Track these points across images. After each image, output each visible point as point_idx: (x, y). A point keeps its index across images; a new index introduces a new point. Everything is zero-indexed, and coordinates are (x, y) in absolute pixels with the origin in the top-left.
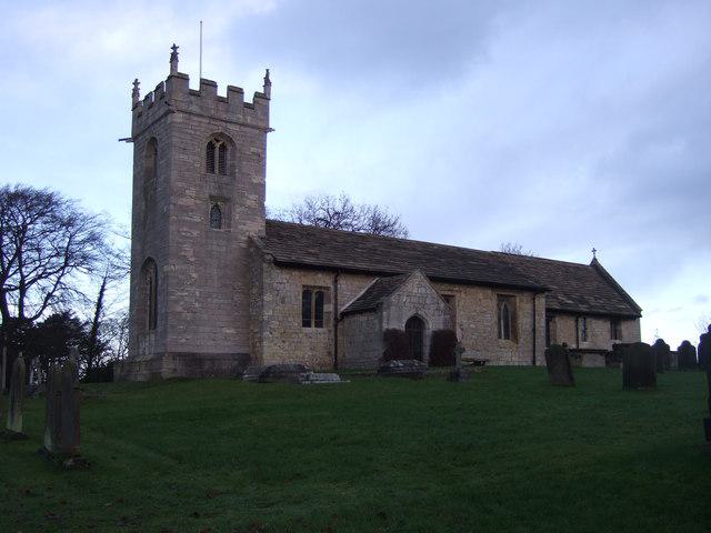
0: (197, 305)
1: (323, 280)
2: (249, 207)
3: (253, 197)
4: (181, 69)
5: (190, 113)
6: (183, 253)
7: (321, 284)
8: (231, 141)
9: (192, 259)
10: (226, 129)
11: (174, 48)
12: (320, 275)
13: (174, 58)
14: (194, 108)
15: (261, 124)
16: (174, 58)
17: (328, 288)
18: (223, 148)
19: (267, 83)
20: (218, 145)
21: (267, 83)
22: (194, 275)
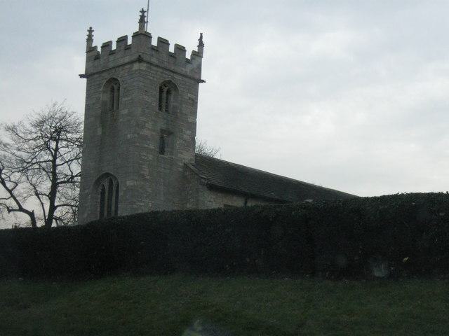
2: (185, 141)
5: (151, 64)
6: (142, 173)
8: (175, 88)
9: (148, 177)
10: (173, 78)
11: (201, 34)
12: (235, 198)
13: (142, 21)
14: (154, 60)
15: (197, 77)
16: (142, 21)
18: (168, 92)
19: (201, 45)
20: (165, 89)
21: (201, 45)
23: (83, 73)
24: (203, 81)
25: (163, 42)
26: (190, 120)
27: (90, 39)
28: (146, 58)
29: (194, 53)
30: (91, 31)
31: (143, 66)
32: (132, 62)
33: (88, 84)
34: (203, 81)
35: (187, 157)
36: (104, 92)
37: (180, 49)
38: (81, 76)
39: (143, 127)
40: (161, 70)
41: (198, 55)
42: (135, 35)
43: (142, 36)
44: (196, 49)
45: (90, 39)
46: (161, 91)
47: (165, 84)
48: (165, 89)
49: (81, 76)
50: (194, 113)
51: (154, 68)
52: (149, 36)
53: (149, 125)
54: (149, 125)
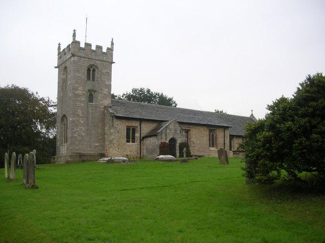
0: (83, 134)
1: (135, 124)
3: (106, 90)
4: (77, 39)
5: (80, 57)
7: (134, 125)
11: (74, 31)
13: (74, 35)
15: (110, 61)
16: (74, 35)
17: (137, 127)
18: (94, 70)
19: (112, 44)
20: (92, 69)
21: (112, 44)
22: (82, 122)
23: (57, 66)
24: (114, 63)
25: (88, 45)
26: (107, 83)
27: (59, 48)
28: (76, 54)
29: (108, 49)
30: (59, 44)
31: (76, 58)
32: (71, 57)
33: (59, 72)
34: (114, 63)
35: (107, 102)
36: (63, 74)
37: (99, 48)
38: (56, 67)
39: (77, 89)
40: (87, 59)
41: (110, 50)
42: (108, 49)
43: (76, 43)
44: (110, 47)
45: (59, 48)
46: (89, 70)
47: (91, 66)
48: (92, 69)
49: (56, 67)
50: (110, 79)
51: (83, 59)
52: (79, 43)
53: (81, 88)
54: (81, 88)
